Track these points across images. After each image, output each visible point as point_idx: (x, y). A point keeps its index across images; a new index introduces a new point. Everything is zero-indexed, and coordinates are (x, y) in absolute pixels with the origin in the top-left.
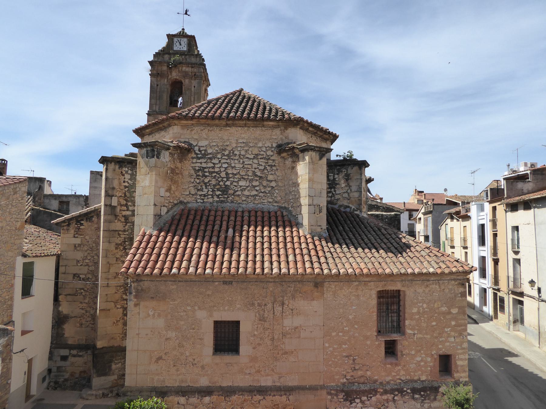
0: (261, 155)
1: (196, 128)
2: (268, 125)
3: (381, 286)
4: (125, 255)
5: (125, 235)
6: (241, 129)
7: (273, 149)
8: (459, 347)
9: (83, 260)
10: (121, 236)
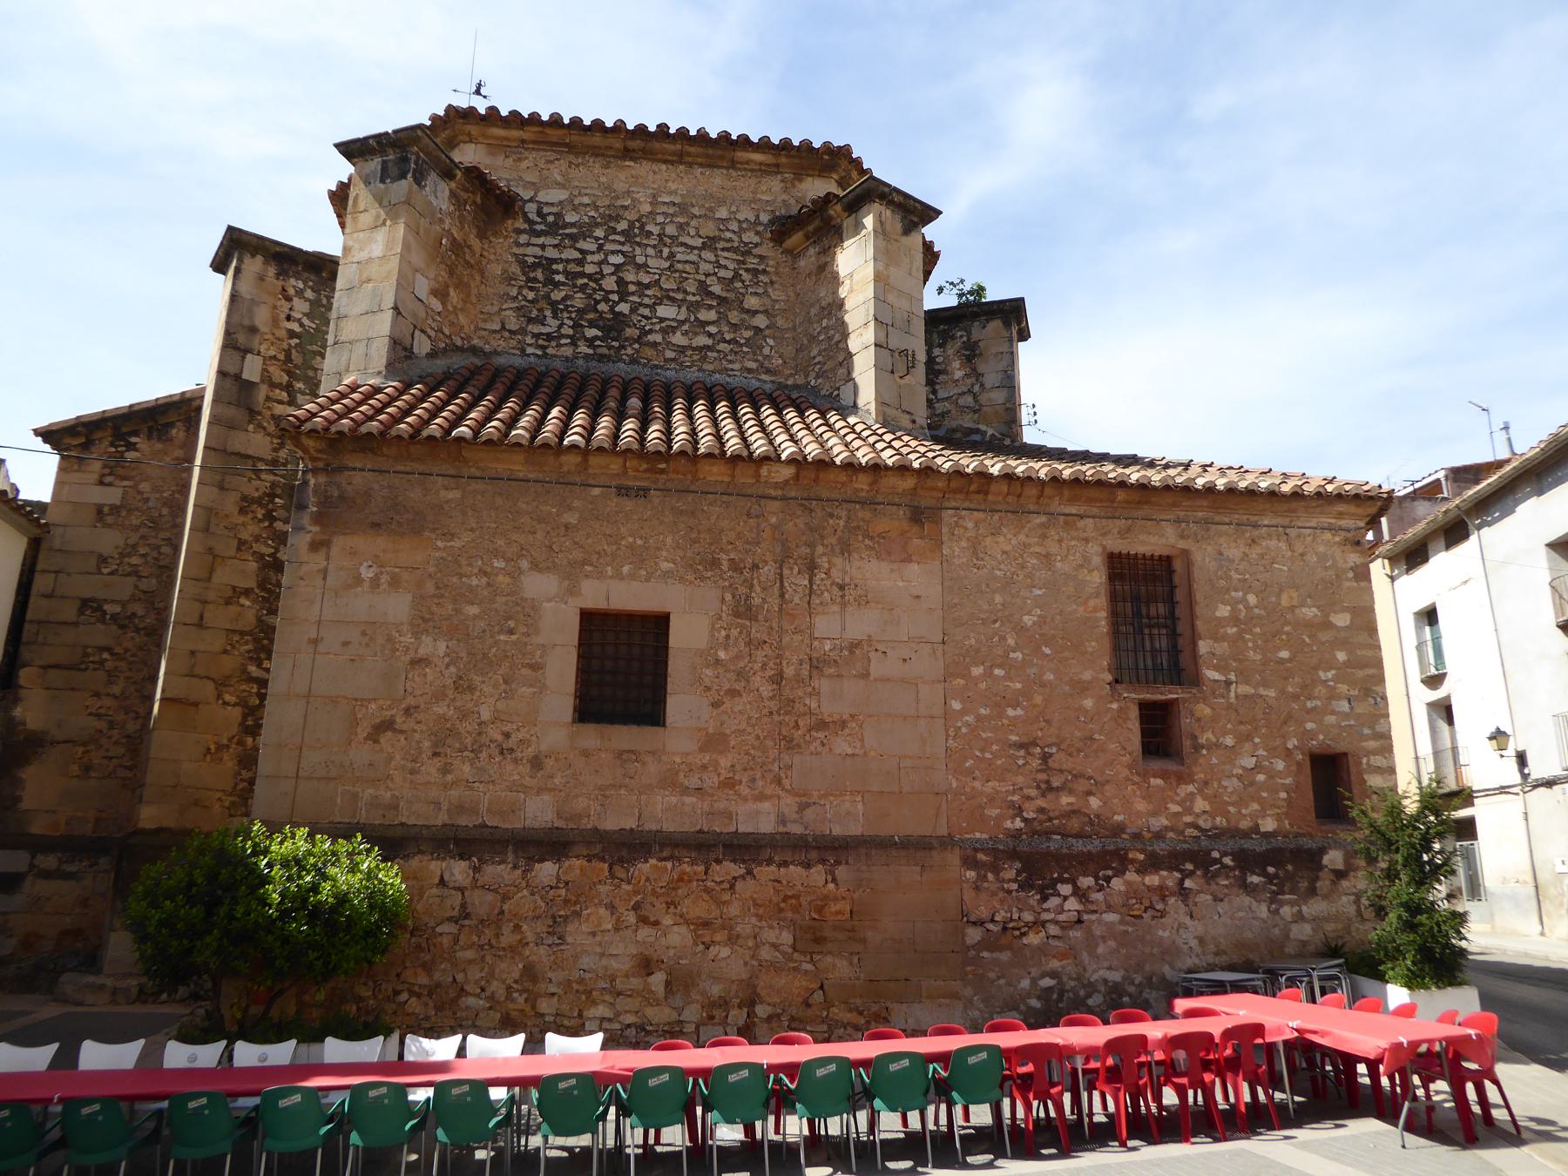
0: (724, 240)
1: (534, 154)
2: (747, 163)
3: (1116, 531)
5: (276, 475)
7: (760, 228)
8: (1367, 731)
9: (122, 555)
10: (263, 476)
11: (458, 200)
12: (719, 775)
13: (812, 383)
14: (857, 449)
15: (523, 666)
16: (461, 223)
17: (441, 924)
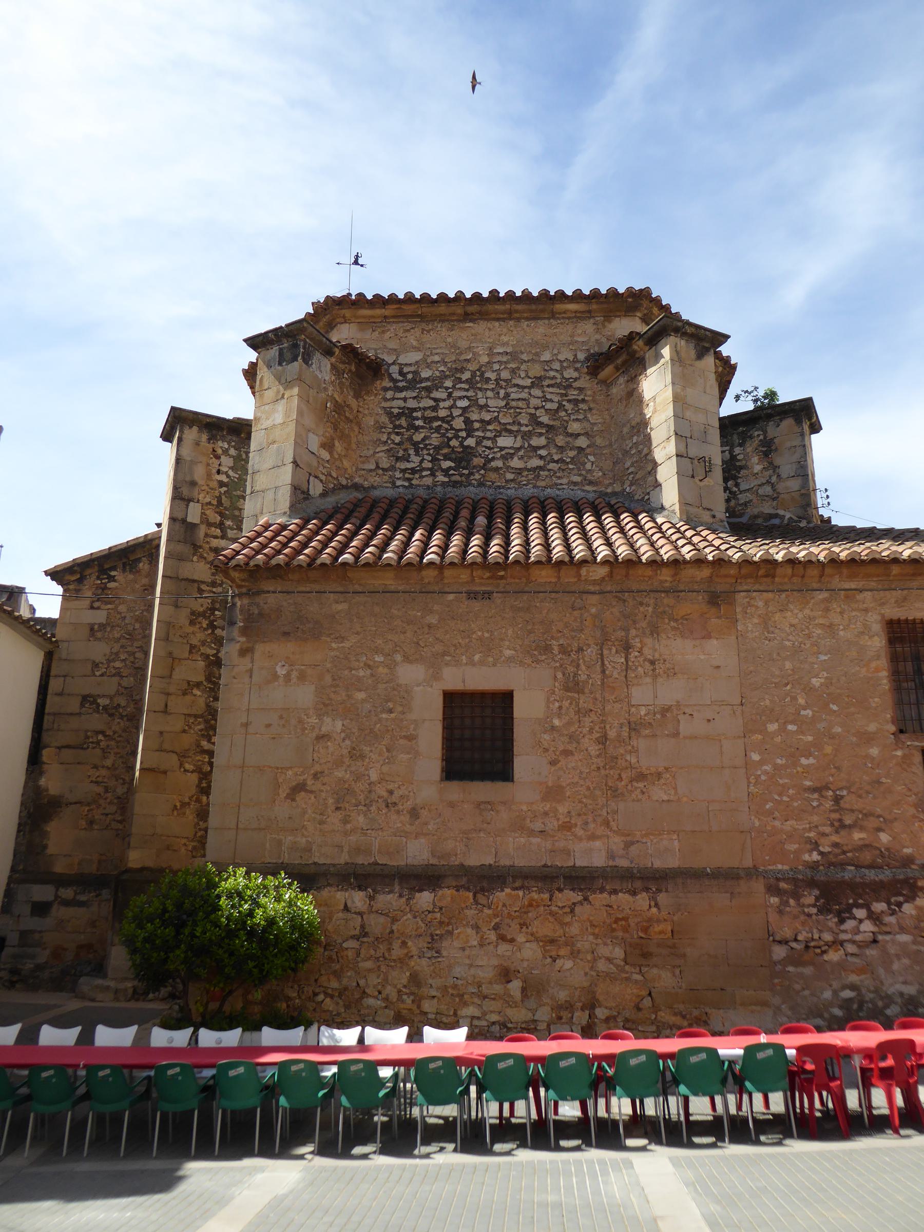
2: (564, 313)
3: (893, 600)
4: (212, 642)
6: (500, 325)
7: (579, 365)
9: (109, 661)
11: (338, 371)
12: (558, 819)
13: (628, 490)
14: (661, 547)
15: (401, 738)
16: (341, 388)
17: (347, 940)
